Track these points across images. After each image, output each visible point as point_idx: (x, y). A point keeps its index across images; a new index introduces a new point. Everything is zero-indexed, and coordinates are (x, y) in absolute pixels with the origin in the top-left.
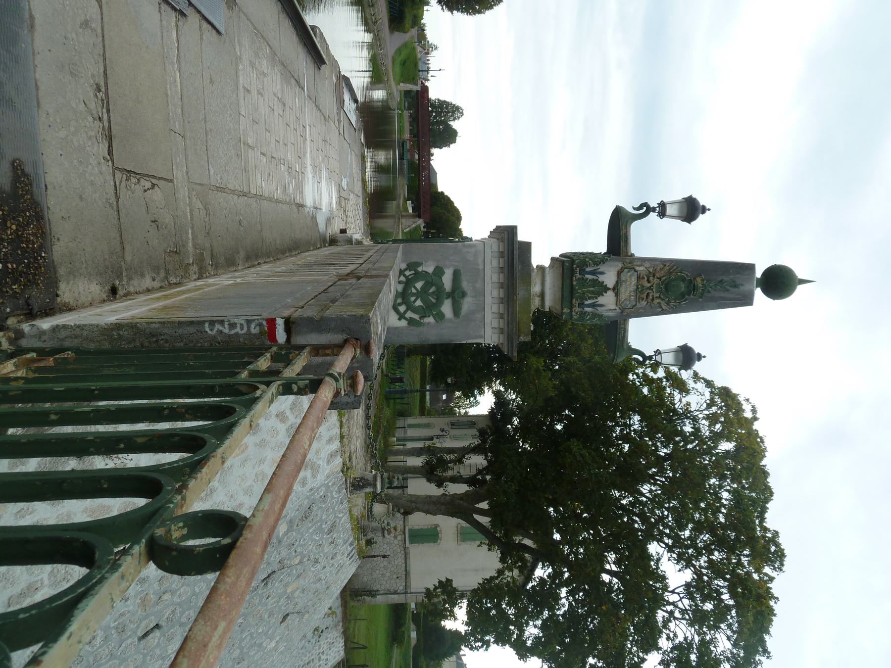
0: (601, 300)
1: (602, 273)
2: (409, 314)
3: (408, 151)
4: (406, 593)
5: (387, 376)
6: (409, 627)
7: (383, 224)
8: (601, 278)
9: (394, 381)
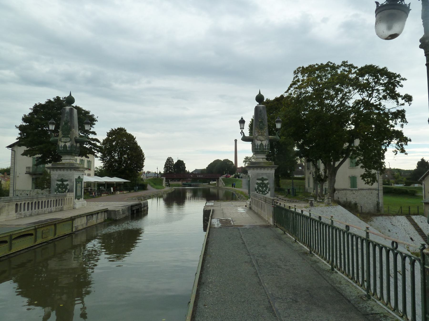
0: (264, 145)
2: (267, 191)
3: (187, 182)
4: (378, 190)
5: (287, 195)
6: (412, 188)
7: (221, 194)
8: (259, 145)
9: (289, 192)
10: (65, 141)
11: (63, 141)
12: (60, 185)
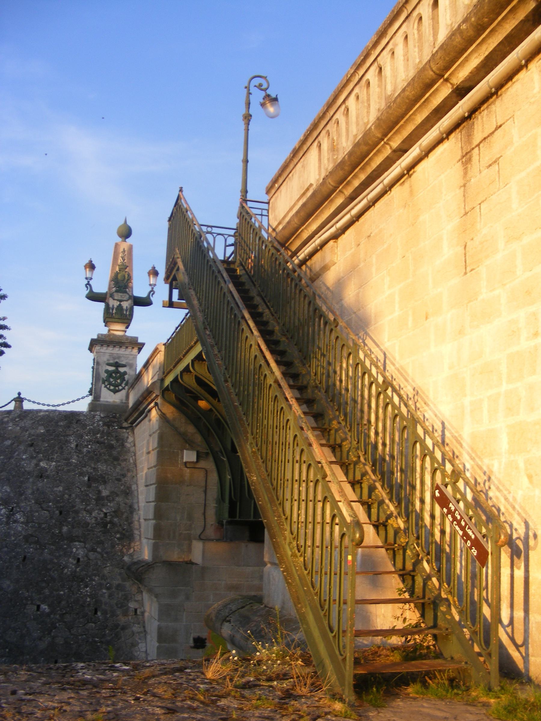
0: (125, 307)
1: (113, 306)
2: (123, 385)
10: (120, 298)
11: (116, 298)
12: (113, 372)
